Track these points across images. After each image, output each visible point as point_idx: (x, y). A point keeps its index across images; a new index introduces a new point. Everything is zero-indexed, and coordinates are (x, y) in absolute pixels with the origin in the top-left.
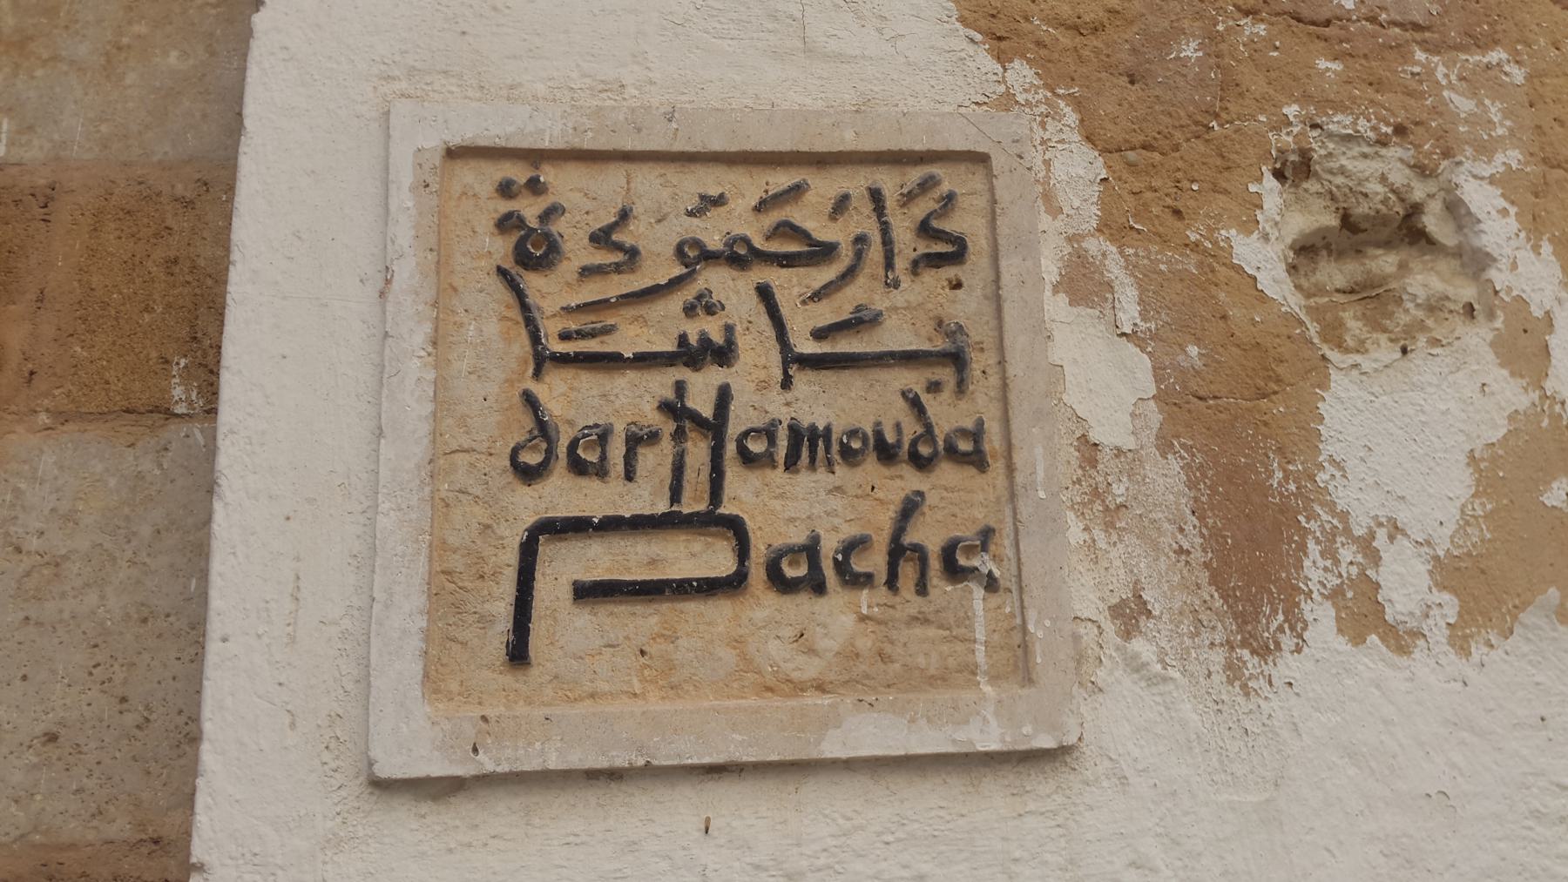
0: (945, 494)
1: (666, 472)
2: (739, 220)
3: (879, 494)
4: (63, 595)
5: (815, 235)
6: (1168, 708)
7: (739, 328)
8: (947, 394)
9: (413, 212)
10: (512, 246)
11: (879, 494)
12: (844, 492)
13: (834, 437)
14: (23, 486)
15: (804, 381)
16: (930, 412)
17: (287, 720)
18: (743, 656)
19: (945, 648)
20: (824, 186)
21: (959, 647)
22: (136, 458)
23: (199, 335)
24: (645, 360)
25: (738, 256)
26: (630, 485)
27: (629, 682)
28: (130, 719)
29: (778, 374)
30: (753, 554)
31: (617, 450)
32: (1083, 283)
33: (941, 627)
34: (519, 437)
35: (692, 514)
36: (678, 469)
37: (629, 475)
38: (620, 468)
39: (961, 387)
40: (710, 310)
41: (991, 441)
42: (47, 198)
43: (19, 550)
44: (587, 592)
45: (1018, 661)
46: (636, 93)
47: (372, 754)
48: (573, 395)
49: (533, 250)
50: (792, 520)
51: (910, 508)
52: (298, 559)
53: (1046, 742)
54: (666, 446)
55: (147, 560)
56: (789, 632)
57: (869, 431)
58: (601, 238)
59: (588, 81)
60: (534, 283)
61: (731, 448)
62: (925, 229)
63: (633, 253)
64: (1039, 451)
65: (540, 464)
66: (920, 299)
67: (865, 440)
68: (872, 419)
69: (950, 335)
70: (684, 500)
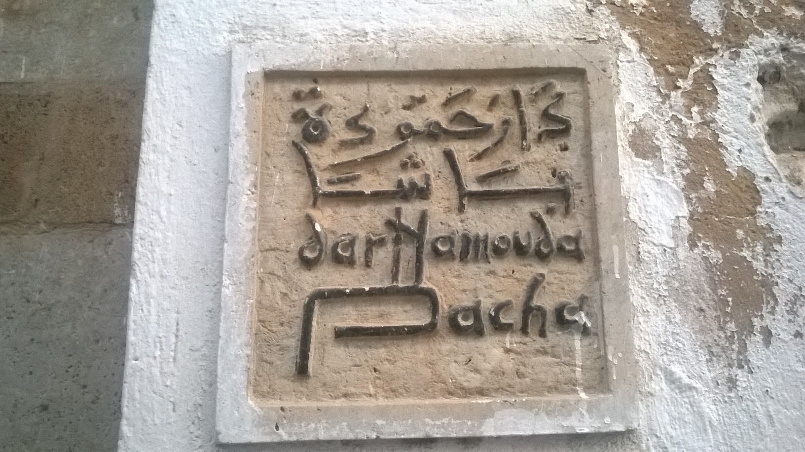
0: (557, 275)
1: (389, 261)
2: (433, 112)
3: (517, 275)
4: (52, 326)
5: (479, 120)
6: (692, 406)
7: (432, 176)
8: (558, 216)
9: (245, 110)
10: (300, 130)
11: (517, 275)
12: (495, 274)
13: (489, 241)
14: (31, 265)
15: (471, 211)
16: (548, 227)
17: (171, 407)
18: (434, 373)
19: (557, 369)
20: (484, 92)
21: (567, 369)
22: (93, 249)
23: (129, 179)
24: (378, 197)
25: (433, 133)
26: (369, 270)
27: (367, 387)
28: (88, 397)
29: (455, 202)
30: (440, 311)
31: (359, 249)
32: (643, 145)
33: (554, 356)
34: (303, 242)
35: (404, 288)
36: (396, 260)
37: (368, 264)
38: (362, 260)
39: (567, 212)
40: (416, 166)
41: (585, 244)
42: (46, 101)
43: (28, 301)
44: (344, 335)
45: (600, 379)
46: (374, 36)
47: (217, 428)
48: (335, 216)
49: (312, 132)
50: (464, 291)
51: (535, 285)
52: (178, 313)
53: (619, 427)
54: (390, 247)
55: (99, 306)
56: (462, 358)
57: (511, 237)
58: (353, 124)
59: (346, 30)
60: (311, 151)
61: (427, 248)
62: (546, 115)
63: (371, 132)
64: (616, 248)
65: (315, 258)
66: (543, 157)
67: (508, 243)
68: (513, 230)
69: (562, 179)
70: (400, 279)
